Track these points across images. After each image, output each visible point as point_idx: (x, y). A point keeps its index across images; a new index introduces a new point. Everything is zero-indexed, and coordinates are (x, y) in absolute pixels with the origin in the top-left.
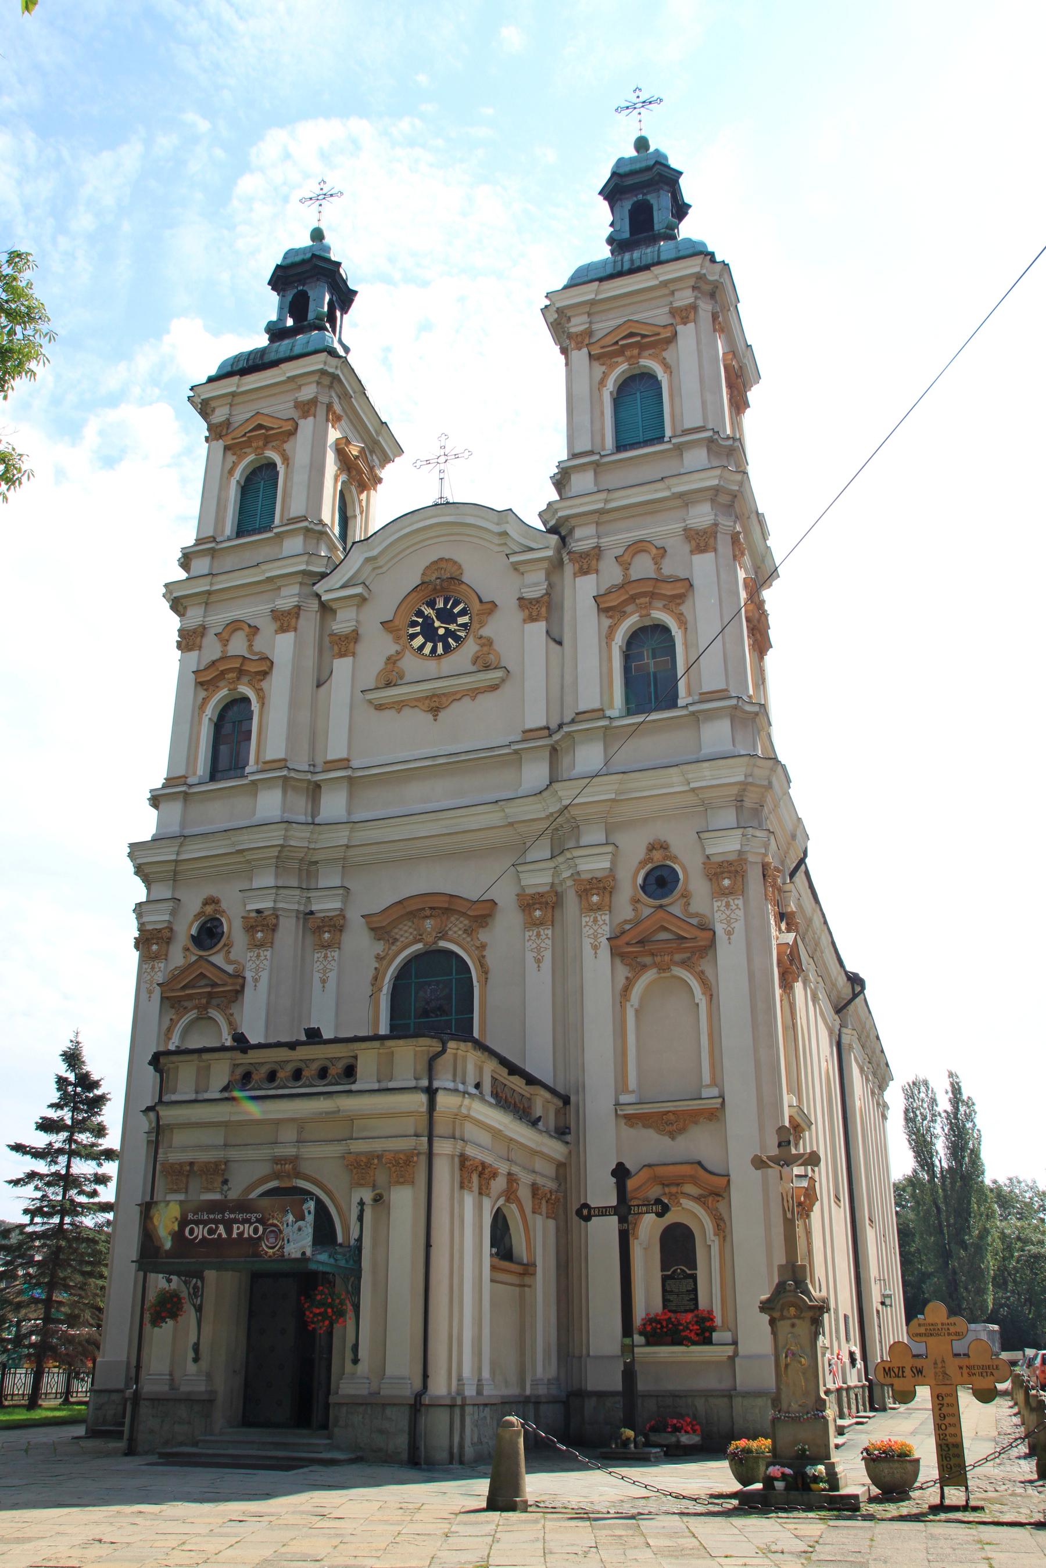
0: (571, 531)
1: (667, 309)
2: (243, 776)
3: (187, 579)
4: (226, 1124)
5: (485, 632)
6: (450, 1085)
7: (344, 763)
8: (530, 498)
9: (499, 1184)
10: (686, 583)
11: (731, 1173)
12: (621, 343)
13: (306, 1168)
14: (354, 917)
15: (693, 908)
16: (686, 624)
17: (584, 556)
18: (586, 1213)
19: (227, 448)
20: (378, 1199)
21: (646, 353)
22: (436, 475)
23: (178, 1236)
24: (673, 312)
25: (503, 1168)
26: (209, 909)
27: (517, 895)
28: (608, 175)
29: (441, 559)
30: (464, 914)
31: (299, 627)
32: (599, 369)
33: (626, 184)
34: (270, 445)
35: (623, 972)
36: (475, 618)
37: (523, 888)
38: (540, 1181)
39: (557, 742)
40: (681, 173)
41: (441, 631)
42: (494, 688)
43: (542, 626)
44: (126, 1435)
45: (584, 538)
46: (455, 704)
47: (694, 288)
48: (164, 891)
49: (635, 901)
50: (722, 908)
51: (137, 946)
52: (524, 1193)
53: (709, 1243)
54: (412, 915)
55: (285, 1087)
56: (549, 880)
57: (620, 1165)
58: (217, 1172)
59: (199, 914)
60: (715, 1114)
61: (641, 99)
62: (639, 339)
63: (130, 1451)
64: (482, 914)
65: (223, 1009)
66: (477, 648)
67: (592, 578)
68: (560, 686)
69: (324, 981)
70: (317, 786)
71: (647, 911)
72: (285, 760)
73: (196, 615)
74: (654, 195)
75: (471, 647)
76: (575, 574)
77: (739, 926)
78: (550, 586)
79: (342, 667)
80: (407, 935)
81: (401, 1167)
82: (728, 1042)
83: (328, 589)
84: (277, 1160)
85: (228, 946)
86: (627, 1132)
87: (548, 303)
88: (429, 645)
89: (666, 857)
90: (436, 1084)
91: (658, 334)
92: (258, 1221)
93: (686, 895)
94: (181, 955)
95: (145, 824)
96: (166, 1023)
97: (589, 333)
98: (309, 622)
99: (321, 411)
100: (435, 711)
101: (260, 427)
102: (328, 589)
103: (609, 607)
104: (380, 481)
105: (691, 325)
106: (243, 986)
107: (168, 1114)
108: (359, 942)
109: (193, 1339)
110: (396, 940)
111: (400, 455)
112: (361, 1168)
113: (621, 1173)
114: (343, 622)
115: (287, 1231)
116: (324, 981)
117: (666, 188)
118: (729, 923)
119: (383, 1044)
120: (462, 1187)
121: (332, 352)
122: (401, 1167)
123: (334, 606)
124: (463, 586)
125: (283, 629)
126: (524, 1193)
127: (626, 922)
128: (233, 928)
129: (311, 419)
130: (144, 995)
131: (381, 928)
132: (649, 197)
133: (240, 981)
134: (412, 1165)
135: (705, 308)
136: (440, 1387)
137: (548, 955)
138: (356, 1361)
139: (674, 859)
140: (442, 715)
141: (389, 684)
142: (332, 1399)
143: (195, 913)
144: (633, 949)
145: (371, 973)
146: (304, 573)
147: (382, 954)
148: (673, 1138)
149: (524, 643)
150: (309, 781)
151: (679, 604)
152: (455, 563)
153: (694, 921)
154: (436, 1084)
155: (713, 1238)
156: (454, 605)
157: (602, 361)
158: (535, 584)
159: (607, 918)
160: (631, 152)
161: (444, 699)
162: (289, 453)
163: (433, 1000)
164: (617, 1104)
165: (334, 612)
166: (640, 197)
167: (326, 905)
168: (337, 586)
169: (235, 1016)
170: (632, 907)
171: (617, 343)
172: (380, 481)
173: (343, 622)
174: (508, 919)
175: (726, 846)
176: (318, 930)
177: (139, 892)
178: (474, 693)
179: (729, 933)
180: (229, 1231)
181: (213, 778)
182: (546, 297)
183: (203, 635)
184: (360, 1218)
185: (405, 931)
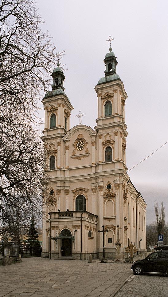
0: (98, 131)
1: (113, 90)
2: (55, 169)
3: (98, 126)
6: (84, 217)
8: (92, 124)
13: (68, 227)
14: (71, 191)
18: (99, 231)
21: (109, 98)
22: (79, 119)
25: (90, 226)
32: (103, 101)
35: (105, 199)
38: (94, 227)
43: (94, 146)
44: (50, 257)
45: (100, 132)
52: (92, 229)
57: (103, 226)
63: (51, 259)
64: (87, 191)
68: (97, 157)
69: (67, 200)
75: (85, 150)
79: (67, 151)
81: (78, 227)
84: (65, 226)
98: (62, 144)
99: (62, 105)
100: (80, 159)
103: (103, 144)
108: (71, 194)
112: (74, 227)
113: (103, 227)
116: (67, 200)
117: (114, 61)
121: (63, 94)
126: (92, 229)
128: (55, 192)
131: (74, 192)
136: (83, 252)
138: (74, 249)
146: (61, 136)
153: (113, 193)
160: (109, 52)
163: (81, 204)
167: (67, 189)
174: (90, 193)
181: (51, 129)
185: (77, 193)
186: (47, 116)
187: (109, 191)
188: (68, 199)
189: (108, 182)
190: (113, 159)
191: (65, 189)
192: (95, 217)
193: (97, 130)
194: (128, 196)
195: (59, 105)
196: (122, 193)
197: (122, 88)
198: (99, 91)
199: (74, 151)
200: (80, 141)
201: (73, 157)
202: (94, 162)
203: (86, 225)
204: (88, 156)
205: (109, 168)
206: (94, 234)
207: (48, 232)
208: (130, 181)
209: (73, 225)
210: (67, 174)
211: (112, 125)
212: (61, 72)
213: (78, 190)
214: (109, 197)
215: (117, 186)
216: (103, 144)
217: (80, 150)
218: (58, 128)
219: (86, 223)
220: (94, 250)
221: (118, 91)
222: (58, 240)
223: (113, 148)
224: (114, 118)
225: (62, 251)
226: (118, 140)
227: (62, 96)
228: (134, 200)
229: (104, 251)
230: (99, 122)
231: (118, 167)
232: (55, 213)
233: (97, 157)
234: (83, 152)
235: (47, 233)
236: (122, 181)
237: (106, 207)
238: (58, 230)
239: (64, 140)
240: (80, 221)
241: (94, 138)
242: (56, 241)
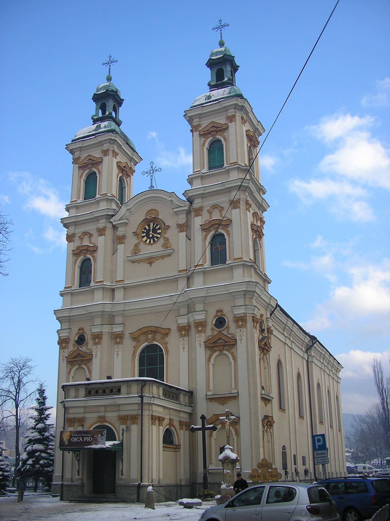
0: (194, 200)
1: (225, 116)
4: (84, 407)
5: (166, 236)
8: (180, 188)
9: (166, 422)
10: (229, 220)
13: (107, 419)
14: (127, 335)
15: (230, 332)
19: (79, 168)
20: (127, 428)
21: (218, 134)
23: (69, 441)
30: (161, 333)
32: (203, 139)
34: (94, 166)
35: (209, 352)
36: (163, 231)
37: (179, 324)
38: (182, 420)
41: (151, 236)
42: (169, 255)
43: (184, 233)
45: (197, 203)
47: (235, 108)
48: (66, 326)
51: (58, 344)
52: (176, 424)
54: (146, 333)
58: (81, 421)
60: (235, 397)
64: (166, 333)
65: (85, 364)
66: (164, 241)
67: (200, 217)
68: (190, 255)
69: (118, 355)
70: (113, 290)
71: (216, 333)
73: (72, 229)
75: (162, 241)
77: (244, 338)
78: (187, 219)
79: (120, 247)
82: (240, 375)
83: (115, 220)
84: (100, 417)
85: (87, 344)
88: (148, 240)
89: (222, 315)
90: (143, 394)
92: (91, 436)
93: (228, 327)
95: (59, 303)
98: (109, 232)
99: (111, 152)
100: (151, 263)
101: (90, 159)
102: (115, 220)
104: (134, 171)
105: (233, 123)
108: (128, 343)
109: (77, 469)
112: (123, 419)
113: (203, 418)
114: (121, 231)
115: (99, 439)
116: (118, 355)
117: (229, 63)
120: (152, 424)
122: (136, 419)
123: (117, 226)
125: (101, 235)
126: (176, 424)
127: (210, 336)
128: (88, 337)
130: (61, 360)
133: (91, 356)
134: (136, 419)
135: (238, 116)
137: (187, 346)
138: (122, 475)
139: (224, 315)
142: (116, 485)
144: (212, 345)
146: (107, 215)
148: (223, 405)
149: (178, 239)
150: (111, 288)
153: (230, 336)
154: (143, 394)
156: (156, 226)
158: (182, 219)
159: (204, 335)
162: (100, 169)
163: (152, 362)
164: (206, 395)
165: (117, 228)
167: (118, 329)
171: (208, 130)
172: (134, 171)
173: (121, 231)
175: (240, 311)
176: (116, 338)
177: (58, 326)
178: (163, 257)
180: (83, 439)
183: (74, 237)
184: (123, 434)
186: (76, 176)
187: (220, 331)
188: (120, 353)
189: (218, 311)
190: (228, 259)
191: (114, 331)
192: (184, 395)
193: (190, 201)
194: (274, 342)
196: (253, 336)
197: (247, 113)
198: (194, 121)
199: (136, 246)
200: (152, 224)
203: (154, 414)
205: (219, 282)
206: (182, 437)
208: (282, 310)
211: (224, 186)
212: (112, 91)
214: (221, 345)
215: (240, 320)
216: (205, 229)
217: (152, 242)
218: (232, 168)
219: (155, 408)
220: (183, 476)
221: (238, 118)
223: (228, 235)
225: (340, 485)
226: (241, 219)
227: (111, 136)
228: (301, 353)
229: (205, 478)
230: (194, 182)
231: (240, 276)
236: (253, 307)
237: (213, 370)
240: (138, 403)
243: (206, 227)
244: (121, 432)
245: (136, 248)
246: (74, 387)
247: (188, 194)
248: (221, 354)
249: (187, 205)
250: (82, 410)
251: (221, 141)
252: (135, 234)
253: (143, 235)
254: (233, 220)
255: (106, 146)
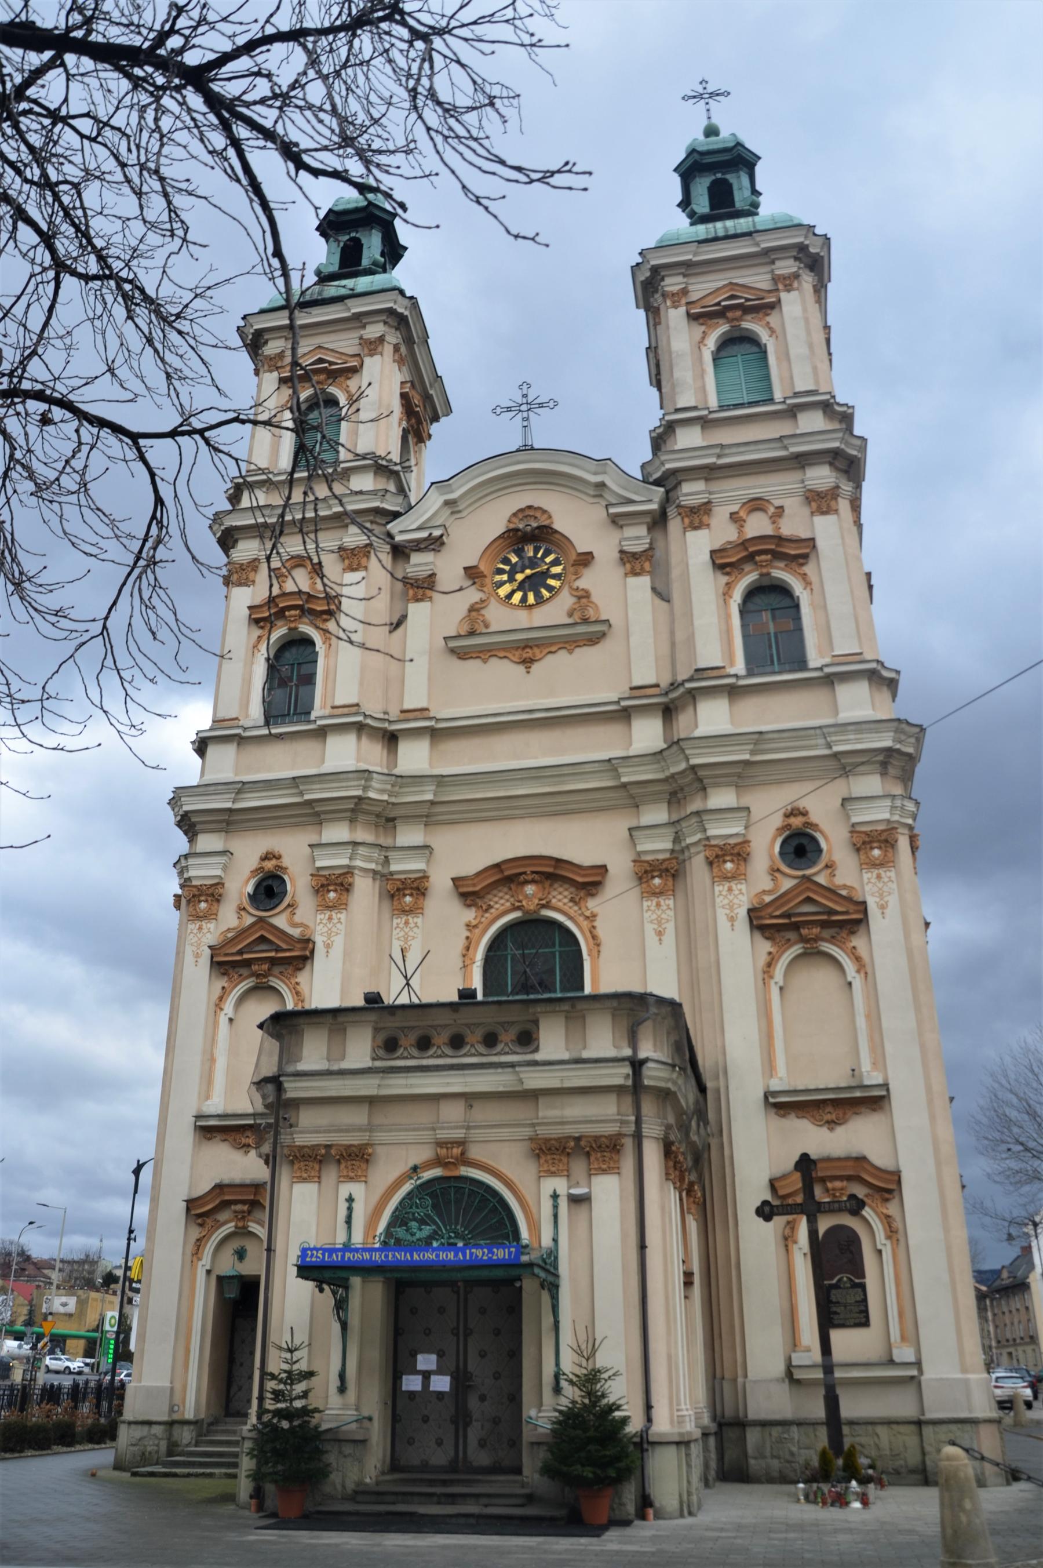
1: (769, 276)
2: (309, 722)
5: (582, 583)
7: (422, 712)
11: (902, 1168)
12: (723, 303)
13: (475, 1152)
14: (440, 882)
16: (811, 584)
17: (693, 511)
24: (775, 279)
26: (269, 865)
27: (634, 861)
28: (683, 156)
29: (530, 507)
31: (257, 581)
32: (699, 330)
33: (704, 161)
39: (673, 701)
40: (759, 158)
43: (645, 581)
45: (692, 491)
46: (550, 656)
49: (774, 871)
50: (873, 880)
53: (879, 1247)
55: (444, 1055)
56: (669, 845)
59: (257, 870)
61: (710, 90)
62: (742, 301)
64: (589, 882)
66: (573, 600)
67: (703, 533)
68: (676, 639)
72: (357, 705)
74: (734, 175)
76: (685, 528)
77: (893, 900)
79: (418, 612)
80: (502, 901)
86: (778, 1123)
87: (640, 260)
91: (762, 299)
94: (235, 916)
96: (217, 992)
97: (685, 292)
103: (724, 563)
106: (312, 952)
107: (293, 1089)
110: (490, 907)
111: (447, 415)
118: (329, 937)
119: (573, 1006)
124: (557, 536)
128: (298, 885)
129: (377, 358)
131: (470, 892)
132: (728, 177)
137: (670, 927)
140: (536, 667)
141: (472, 633)
143: (253, 868)
144: (769, 923)
145: (461, 943)
147: (474, 923)
149: (623, 598)
151: (802, 565)
152: (544, 512)
155: (884, 1241)
157: (701, 321)
158: (637, 537)
161: (536, 651)
166: (719, 175)
167: (403, 865)
168: (414, 527)
169: (302, 985)
170: (770, 877)
179: (883, 907)
182: (640, 254)
185: (501, 901)
191: (394, 867)
195: (373, 346)
201: (469, 646)
202: (652, 681)
204: (594, 640)
207: (209, 1222)
209: (543, 1131)
210: (414, 757)
213: (507, 875)
214: (811, 924)
216: (724, 563)
222: (356, 1281)
224: (794, 416)
232: (335, 1012)
233: (676, 639)
234: (555, 612)
235: (195, 1233)
238: (357, 1189)
239: (398, 538)
241: (642, 531)
242: (341, 1305)
243: (733, 560)
244: (547, 1206)
245: (474, 614)
246: (329, 1019)
247: (663, 464)
248: (812, 954)
249: (657, 499)
250: (358, 1116)
251: (310, 642)
252: (472, 573)
253: (498, 578)
254: (820, 543)
255: (374, 331)
